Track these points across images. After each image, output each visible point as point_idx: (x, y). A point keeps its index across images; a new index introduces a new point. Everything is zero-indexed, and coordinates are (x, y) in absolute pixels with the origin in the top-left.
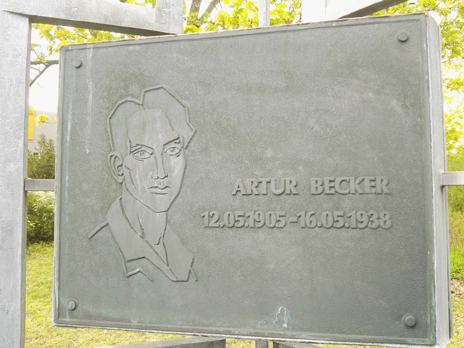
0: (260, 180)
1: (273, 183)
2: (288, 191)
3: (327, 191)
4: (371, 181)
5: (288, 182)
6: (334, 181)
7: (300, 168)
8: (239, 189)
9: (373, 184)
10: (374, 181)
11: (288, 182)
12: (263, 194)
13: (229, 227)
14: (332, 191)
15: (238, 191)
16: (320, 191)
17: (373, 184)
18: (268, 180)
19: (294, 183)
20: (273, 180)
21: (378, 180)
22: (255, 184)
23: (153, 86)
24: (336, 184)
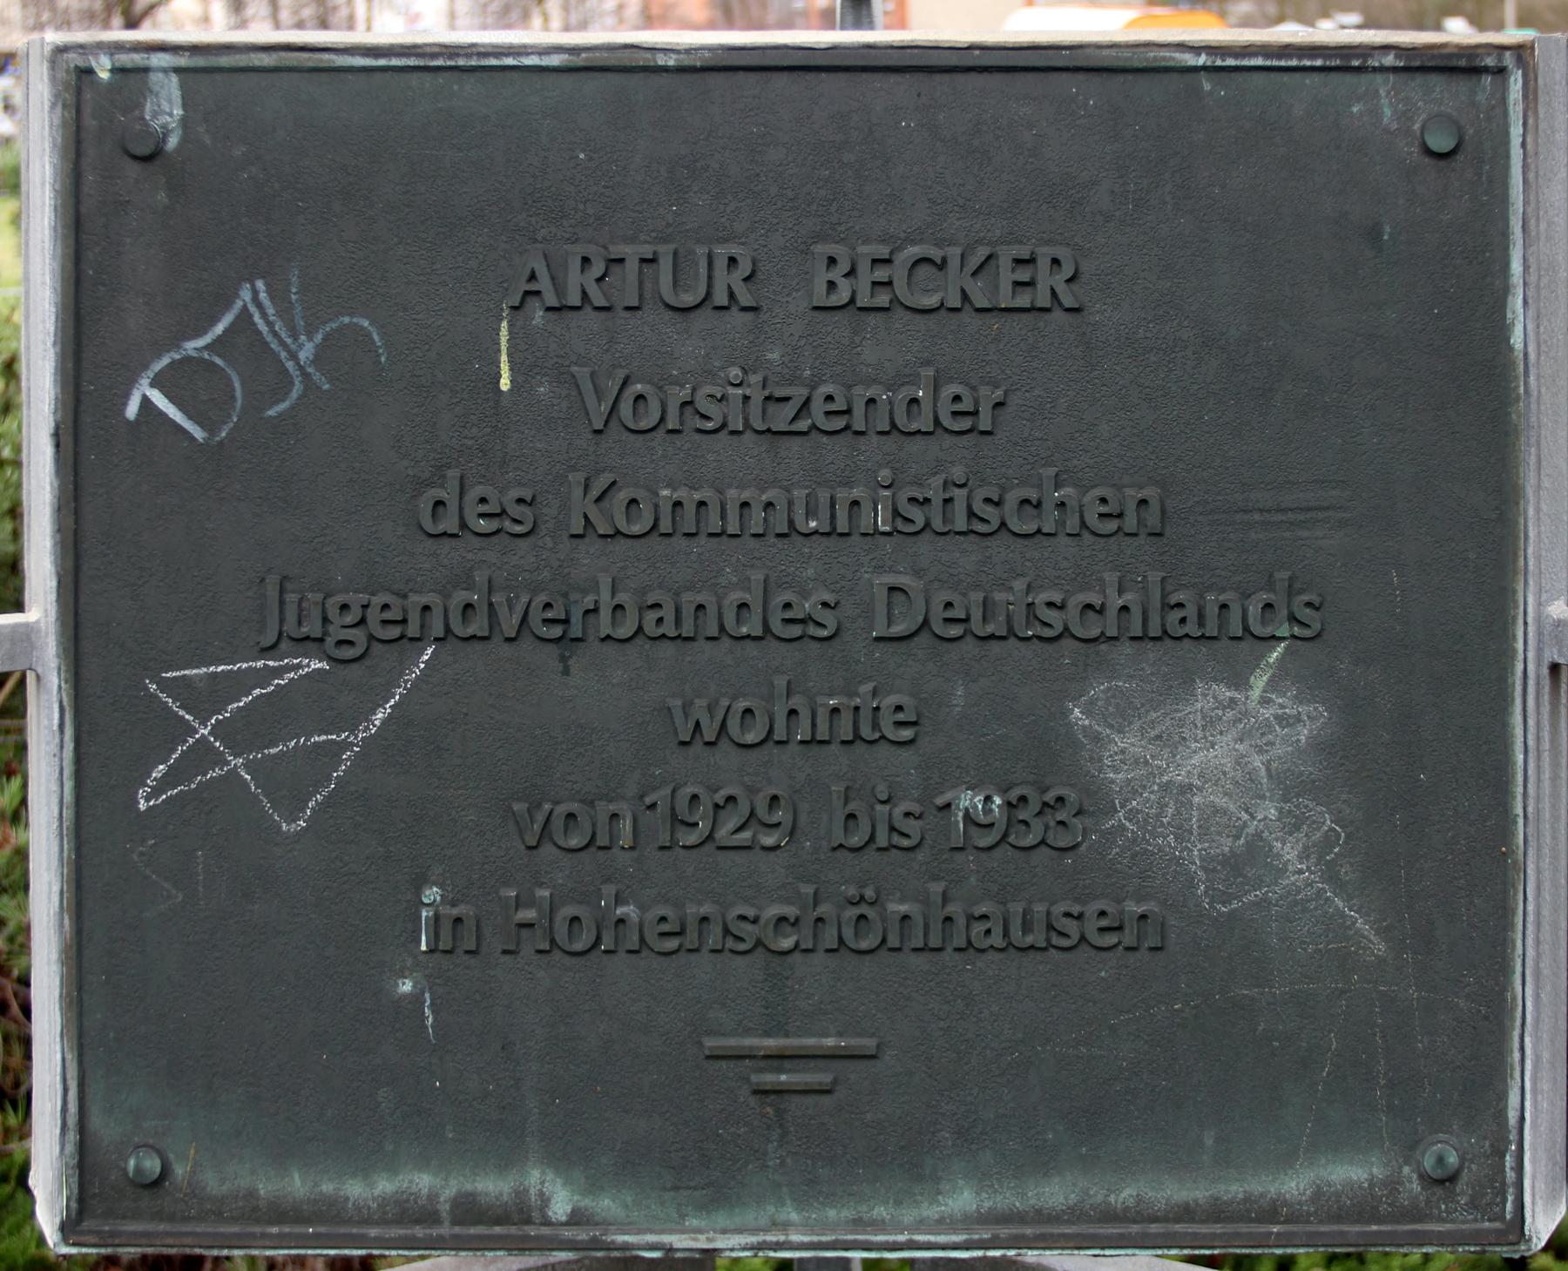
0: (617, 250)
1: (666, 265)
2: (721, 298)
3: (862, 301)
4: (1018, 262)
5: (721, 264)
6: (888, 261)
7: (1355, 109)
8: (533, 287)
9: (1023, 275)
10: (888, 261)
11: (721, 264)
12: (628, 308)
13: (135, 158)
14: (883, 299)
15: (527, 293)
16: (843, 296)
17: (1023, 275)
18: (647, 251)
19: (745, 268)
20: (665, 251)
21: (1043, 264)
22: (598, 269)
23: (1534, 1091)
24: (899, 273)
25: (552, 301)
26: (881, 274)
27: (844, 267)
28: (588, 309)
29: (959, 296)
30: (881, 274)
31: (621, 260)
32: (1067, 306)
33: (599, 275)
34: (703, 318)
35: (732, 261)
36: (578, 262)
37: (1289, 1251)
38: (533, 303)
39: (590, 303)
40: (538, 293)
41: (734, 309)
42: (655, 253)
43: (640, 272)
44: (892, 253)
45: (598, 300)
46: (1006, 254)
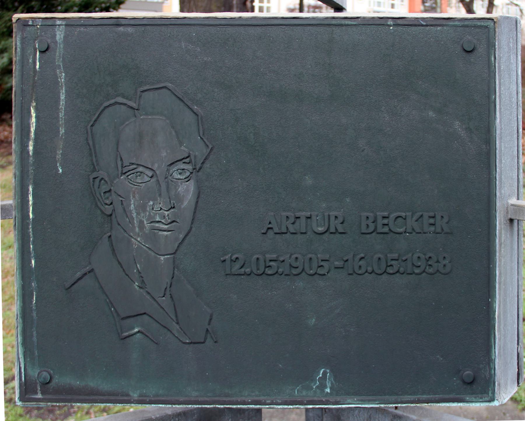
0: (298, 214)
2: (332, 230)
6: (387, 217)
8: (270, 226)
9: (432, 221)
11: (332, 218)
14: (386, 229)
15: (269, 228)
16: (371, 229)
19: (340, 219)
21: (438, 217)
22: (292, 220)
25: (276, 230)
26: (385, 221)
27: (371, 219)
28: (414, 233)
29: (335, 229)
30: (385, 221)
31: (299, 218)
32: (291, 232)
33: (447, 220)
34: (325, 237)
35: (336, 217)
36: (334, 218)
37: (258, 406)
38: (270, 231)
39: (415, 231)
40: (271, 228)
41: (288, 233)
42: (311, 215)
43: (307, 222)
44: (389, 214)
45: (292, 230)
46: (426, 215)
